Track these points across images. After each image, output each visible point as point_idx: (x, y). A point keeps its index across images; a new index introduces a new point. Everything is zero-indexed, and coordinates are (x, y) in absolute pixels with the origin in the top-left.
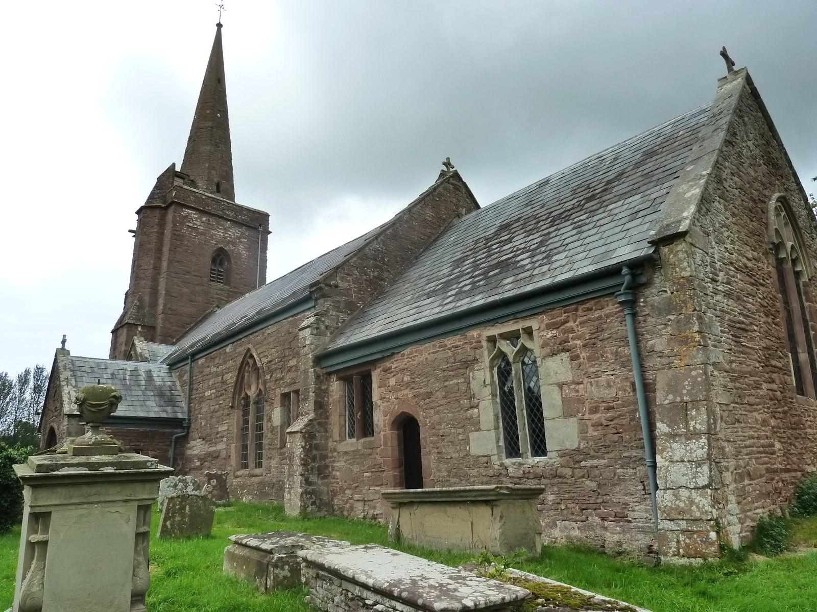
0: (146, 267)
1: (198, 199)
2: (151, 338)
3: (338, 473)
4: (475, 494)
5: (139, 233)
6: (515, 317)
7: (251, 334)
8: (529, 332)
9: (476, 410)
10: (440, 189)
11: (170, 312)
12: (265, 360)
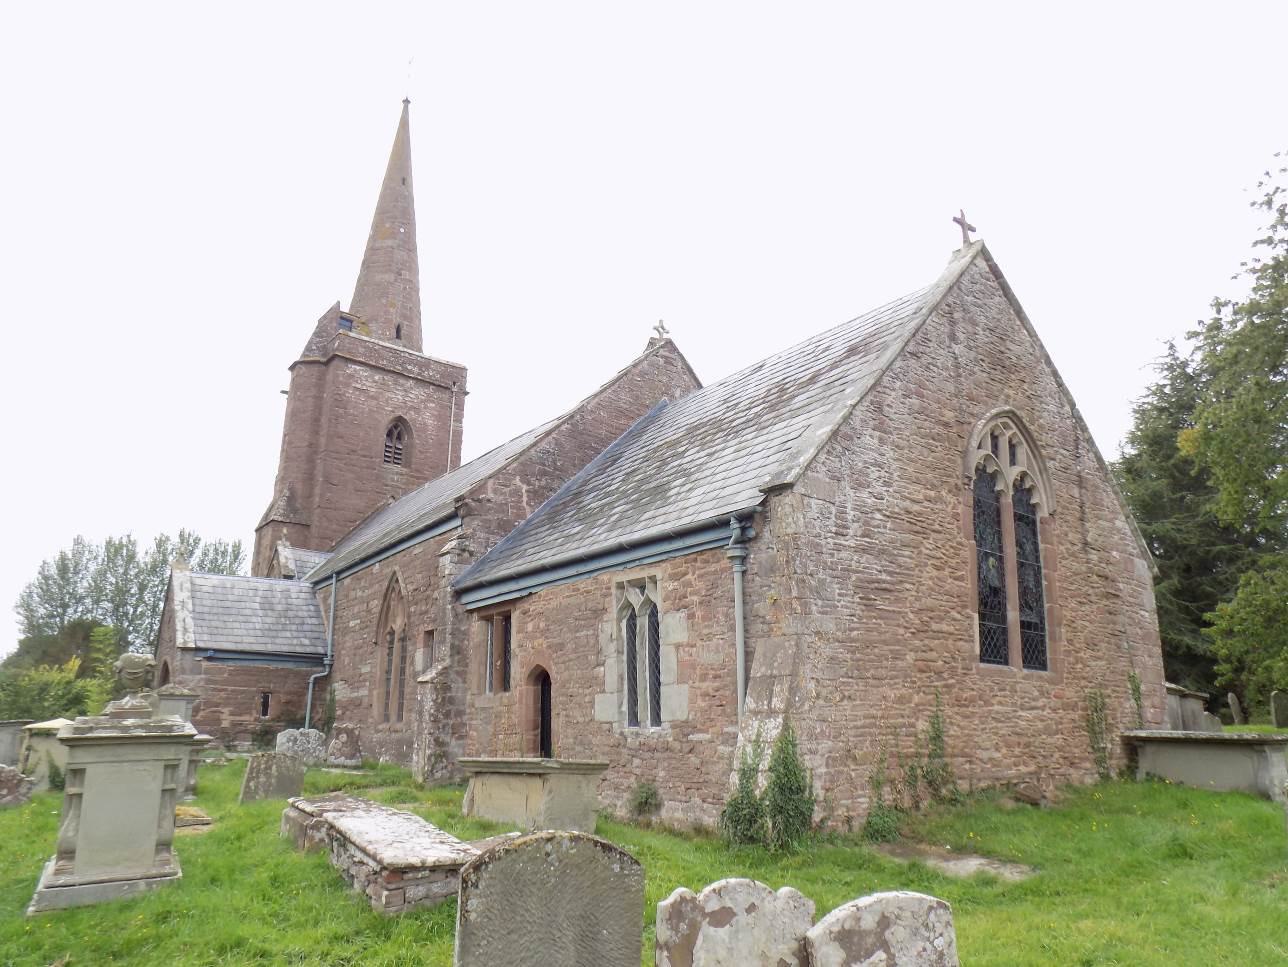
1: (371, 350)
2: (301, 543)
3: (475, 734)
4: (527, 766)
5: (295, 393)
8: (653, 579)
9: (602, 669)
12: (411, 588)
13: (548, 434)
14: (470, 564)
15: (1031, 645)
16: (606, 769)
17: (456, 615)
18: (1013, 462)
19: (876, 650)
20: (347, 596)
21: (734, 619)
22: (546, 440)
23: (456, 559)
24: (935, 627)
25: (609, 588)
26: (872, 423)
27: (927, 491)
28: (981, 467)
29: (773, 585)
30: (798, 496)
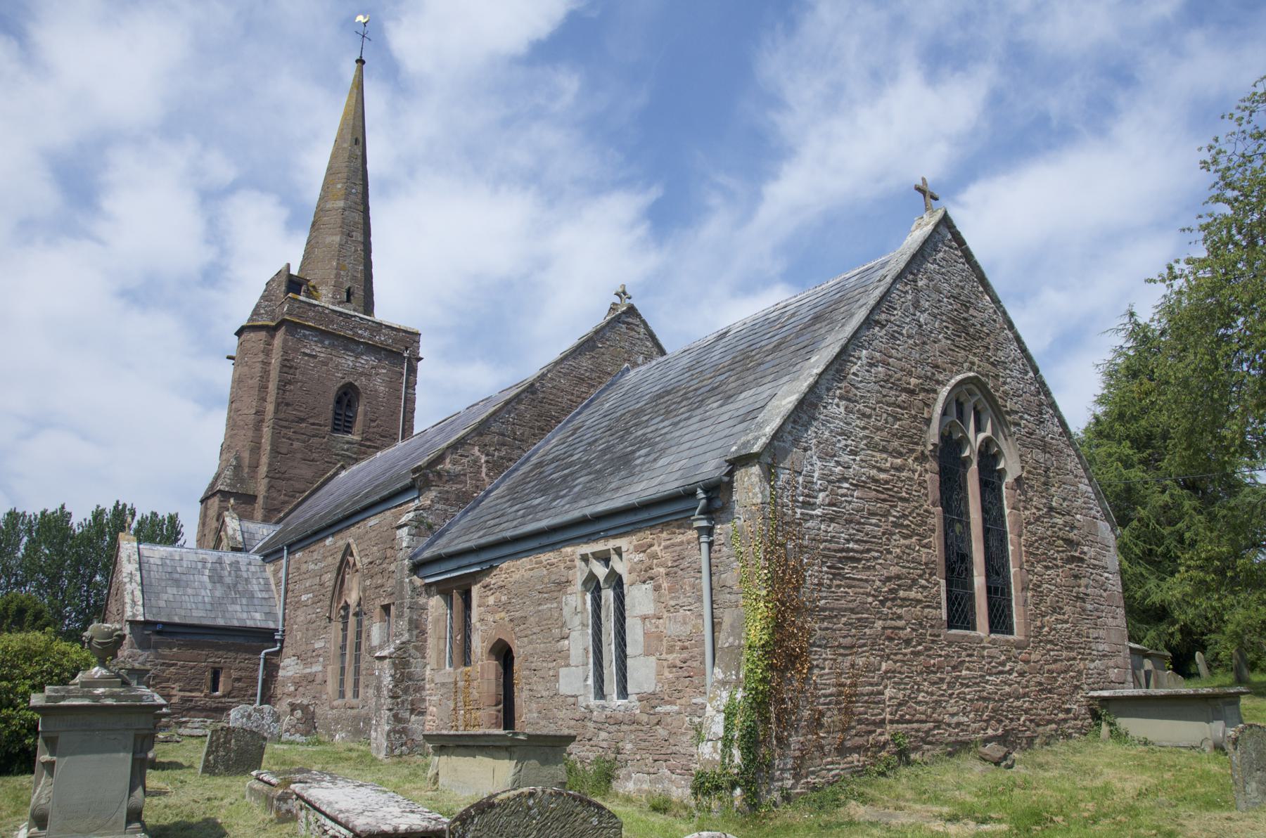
0: (246, 412)
8: (618, 552)
9: (566, 642)
12: (366, 561)
15: (997, 610)
17: (414, 589)
20: (299, 569)
24: (902, 594)
28: (946, 434)
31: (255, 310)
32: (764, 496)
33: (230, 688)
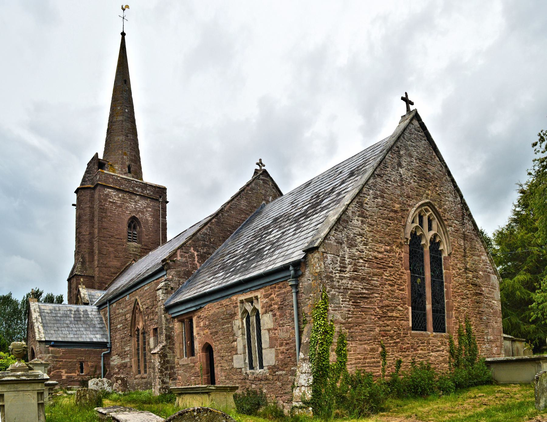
2: (90, 286)
3: (180, 377)
4: (201, 389)
6: (250, 290)
7: (138, 289)
8: (256, 298)
9: (236, 343)
10: (253, 185)
11: (102, 266)
12: (145, 307)
13: (206, 224)
14: (172, 294)
15: (438, 321)
16: (237, 389)
17: (167, 320)
18: (430, 229)
19: (361, 327)
20: (115, 312)
21: (293, 315)
22: (205, 228)
23: (164, 292)
24: (390, 314)
25: (236, 303)
26: (358, 213)
27: (386, 247)
28: (413, 233)
29: (311, 298)
30: (321, 253)
31: (83, 179)
32: (321, 268)
33: (88, 371)
